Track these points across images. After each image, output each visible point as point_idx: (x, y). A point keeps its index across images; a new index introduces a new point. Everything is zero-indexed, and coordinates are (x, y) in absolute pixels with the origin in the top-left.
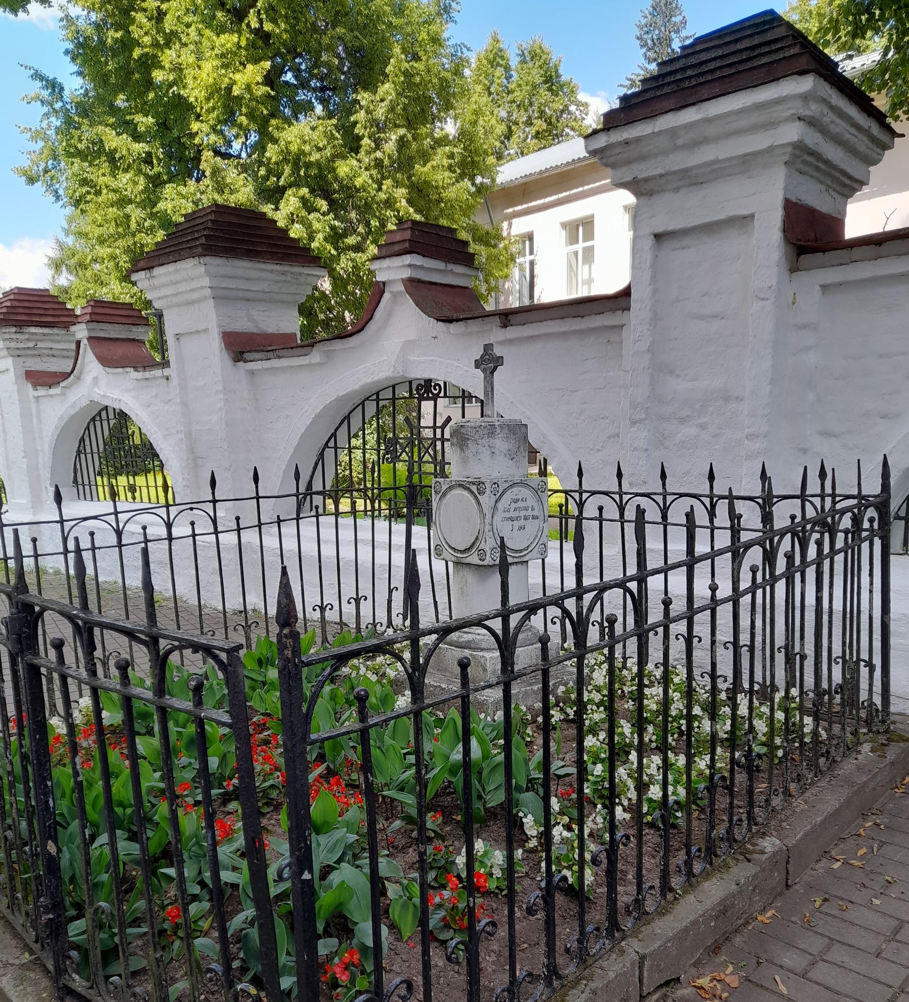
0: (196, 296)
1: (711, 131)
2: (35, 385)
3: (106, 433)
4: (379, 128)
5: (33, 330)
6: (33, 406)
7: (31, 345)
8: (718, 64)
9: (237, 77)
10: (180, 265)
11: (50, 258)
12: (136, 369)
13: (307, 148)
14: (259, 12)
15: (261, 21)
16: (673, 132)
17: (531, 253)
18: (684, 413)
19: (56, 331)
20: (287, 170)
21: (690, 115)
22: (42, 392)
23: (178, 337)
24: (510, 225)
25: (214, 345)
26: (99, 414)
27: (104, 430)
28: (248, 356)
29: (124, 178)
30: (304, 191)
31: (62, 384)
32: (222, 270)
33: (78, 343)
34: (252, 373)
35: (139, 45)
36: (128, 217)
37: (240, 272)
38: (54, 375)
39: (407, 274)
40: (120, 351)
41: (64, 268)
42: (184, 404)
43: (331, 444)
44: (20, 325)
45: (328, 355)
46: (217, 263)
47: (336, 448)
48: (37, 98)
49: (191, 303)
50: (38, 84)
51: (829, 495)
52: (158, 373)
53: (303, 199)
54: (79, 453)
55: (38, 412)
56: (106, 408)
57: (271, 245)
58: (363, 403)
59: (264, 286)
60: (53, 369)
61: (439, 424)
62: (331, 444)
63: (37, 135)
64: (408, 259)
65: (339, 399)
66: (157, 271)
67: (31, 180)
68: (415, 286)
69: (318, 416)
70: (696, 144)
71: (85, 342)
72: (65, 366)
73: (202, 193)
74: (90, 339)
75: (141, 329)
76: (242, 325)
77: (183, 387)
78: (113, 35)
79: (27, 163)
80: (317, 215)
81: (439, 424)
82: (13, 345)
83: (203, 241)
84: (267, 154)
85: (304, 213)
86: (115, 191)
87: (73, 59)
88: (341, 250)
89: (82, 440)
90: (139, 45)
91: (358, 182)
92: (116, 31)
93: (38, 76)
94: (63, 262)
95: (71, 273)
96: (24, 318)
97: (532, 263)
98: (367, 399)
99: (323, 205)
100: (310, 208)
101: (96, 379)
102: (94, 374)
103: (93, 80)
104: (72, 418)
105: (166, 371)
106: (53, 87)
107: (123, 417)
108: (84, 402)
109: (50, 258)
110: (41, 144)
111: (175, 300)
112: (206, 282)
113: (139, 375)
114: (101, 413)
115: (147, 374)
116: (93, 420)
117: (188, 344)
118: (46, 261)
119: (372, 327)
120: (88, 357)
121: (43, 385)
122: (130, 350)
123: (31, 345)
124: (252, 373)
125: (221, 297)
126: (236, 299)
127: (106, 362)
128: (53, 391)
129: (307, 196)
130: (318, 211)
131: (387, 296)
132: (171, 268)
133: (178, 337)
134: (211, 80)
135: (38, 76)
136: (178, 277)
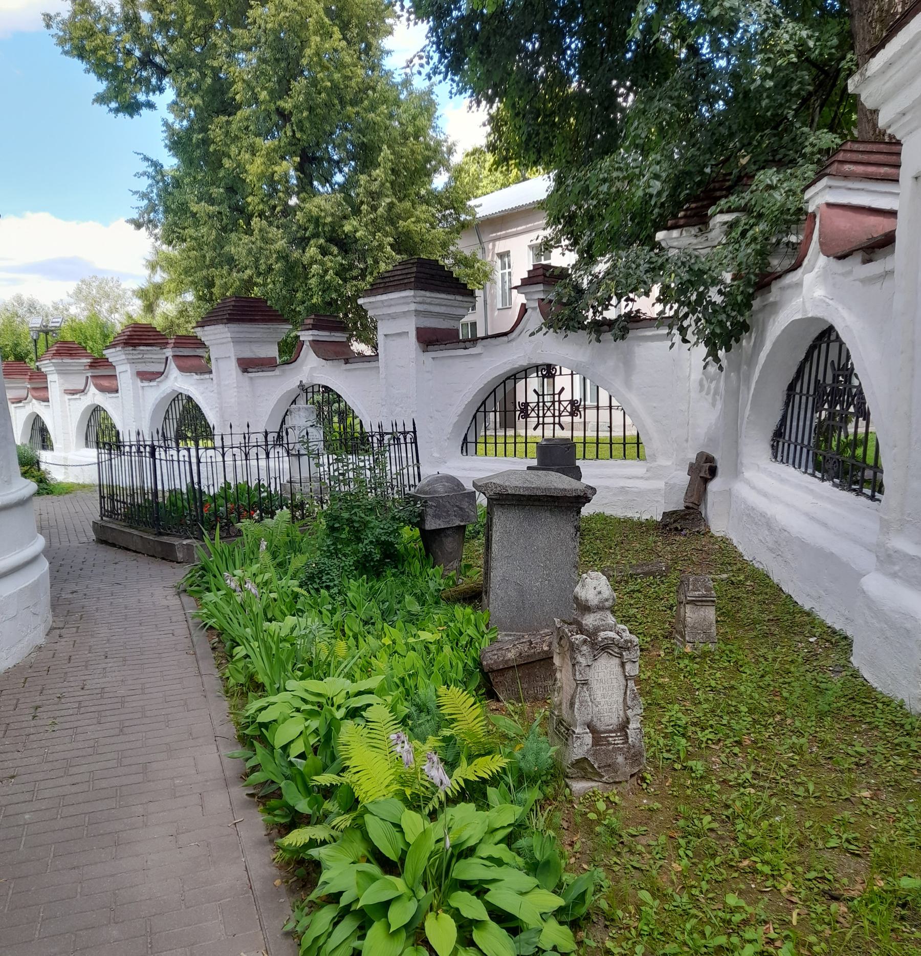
0: (224, 341)
1: (392, 302)
2: (142, 380)
3: (181, 408)
4: (375, 196)
5: (142, 348)
6: (141, 392)
7: (140, 356)
8: (401, 277)
9: (276, 168)
10: (216, 327)
11: (148, 261)
12: (196, 374)
13: (323, 214)
14: (292, 124)
15: (294, 132)
16: (382, 301)
17: (509, 267)
18: (397, 402)
19: (154, 348)
20: (311, 227)
21: (384, 297)
22: (146, 384)
23: (217, 359)
24: (494, 246)
25: (233, 364)
26: (177, 396)
27: (179, 406)
28: (250, 370)
29: (204, 230)
30: (322, 241)
31: (158, 380)
32: (236, 329)
33: (167, 358)
34: (251, 378)
35: (213, 142)
36: (204, 256)
37: (246, 330)
38: (153, 373)
39: (311, 338)
40: (189, 362)
41: (158, 269)
42: (219, 393)
43: (482, 409)
44: (135, 345)
45: (283, 371)
46: (234, 327)
47: (485, 412)
48: (144, 174)
49: (223, 343)
50: (146, 164)
51: (870, 468)
52: (207, 376)
53: (320, 247)
54: (165, 418)
55: (143, 395)
56: (181, 394)
57: (262, 315)
58: (504, 382)
59: (258, 335)
60: (152, 370)
61: (557, 391)
62: (482, 409)
63: (144, 196)
64: (310, 332)
65: (288, 392)
66: (206, 328)
67: (138, 226)
68: (315, 344)
69: (279, 400)
70: (390, 306)
71: (170, 358)
72: (160, 368)
73: (253, 243)
74: (174, 356)
75: (201, 350)
76: (249, 352)
77: (219, 385)
78: (197, 137)
79: (136, 216)
80: (330, 257)
81: (557, 391)
82: (130, 357)
83: (227, 316)
84: (297, 217)
85: (320, 257)
86: (195, 239)
87: (170, 150)
88: (345, 280)
89: (168, 411)
90: (213, 142)
91: (358, 234)
92: (199, 133)
93: (146, 159)
94: (158, 264)
95: (164, 271)
96: (137, 341)
97: (510, 273)
98: (508, 378)
99: (335, 250)
100: (324, 252)
101: (176, 378)
102: (175, 375)
103: (183, 162)
104: (163, 399)
105: (211, 376)
106: (156, 167)
107: (189, 399)
108: (169, 391)
109: (148, 261)
110: (146, 202)
111: (215, 342)
112: (229, 335)
113: (197, 377)
114: (177, 397)
115: (202, 377)
116: (174, 400)
117: (222, 364)
118: (144, 262)
119: (299, 359)
120: (172, 365)
121: (146, 380)
122: (195, 362)
123: (140, 356)
124: (251, 378)
125: (236, 341)
126: (244, 342)
127: (182, 369)
128: (152, 384)
129: (324, 244)
130: (331, 254)
131: (305, 346)
132: (212, 327)
133: (217, 359)
134: (259, 171)
135: (146, 159)
136: (216, 332)
